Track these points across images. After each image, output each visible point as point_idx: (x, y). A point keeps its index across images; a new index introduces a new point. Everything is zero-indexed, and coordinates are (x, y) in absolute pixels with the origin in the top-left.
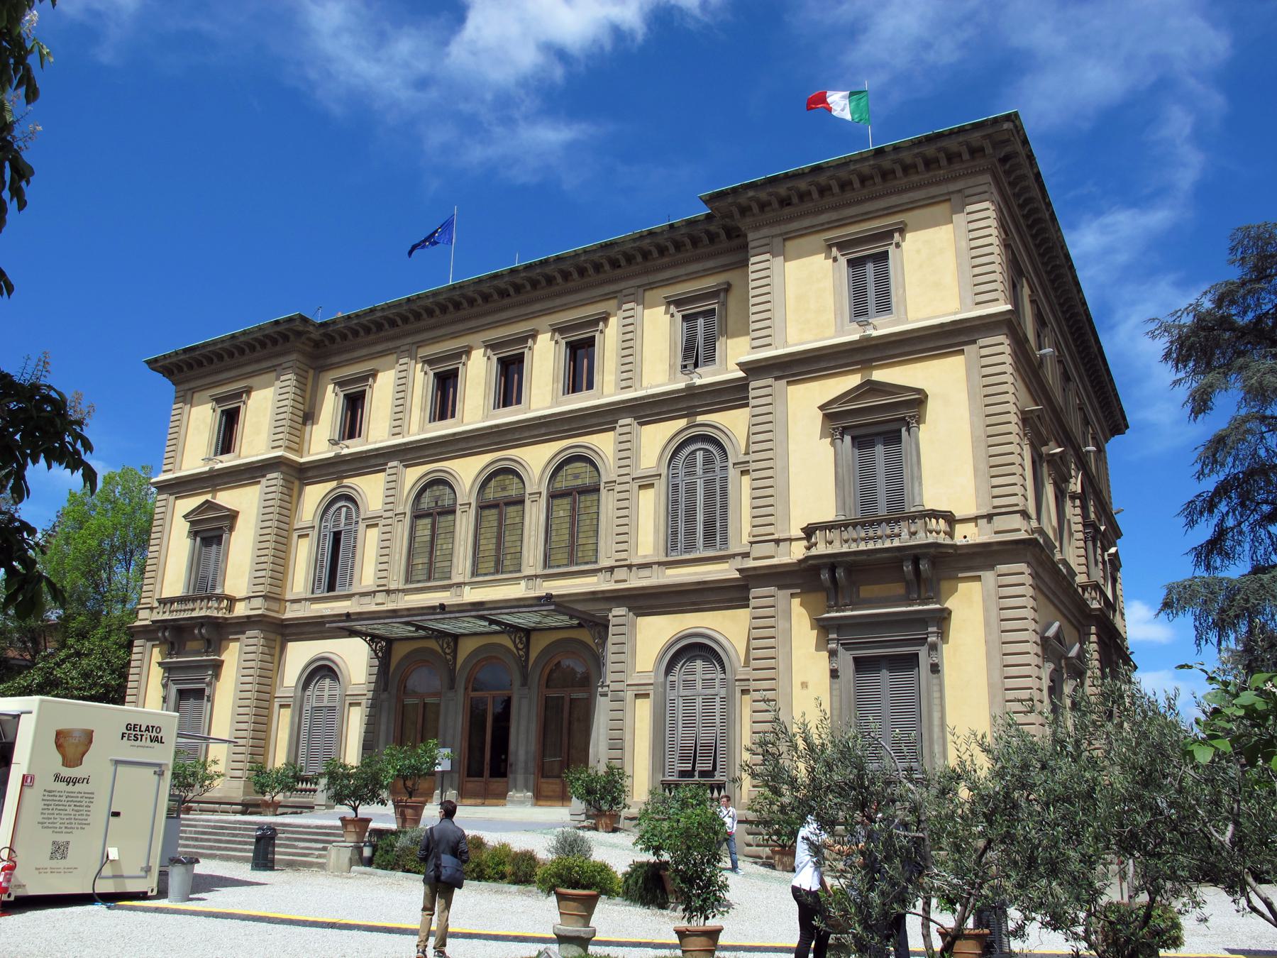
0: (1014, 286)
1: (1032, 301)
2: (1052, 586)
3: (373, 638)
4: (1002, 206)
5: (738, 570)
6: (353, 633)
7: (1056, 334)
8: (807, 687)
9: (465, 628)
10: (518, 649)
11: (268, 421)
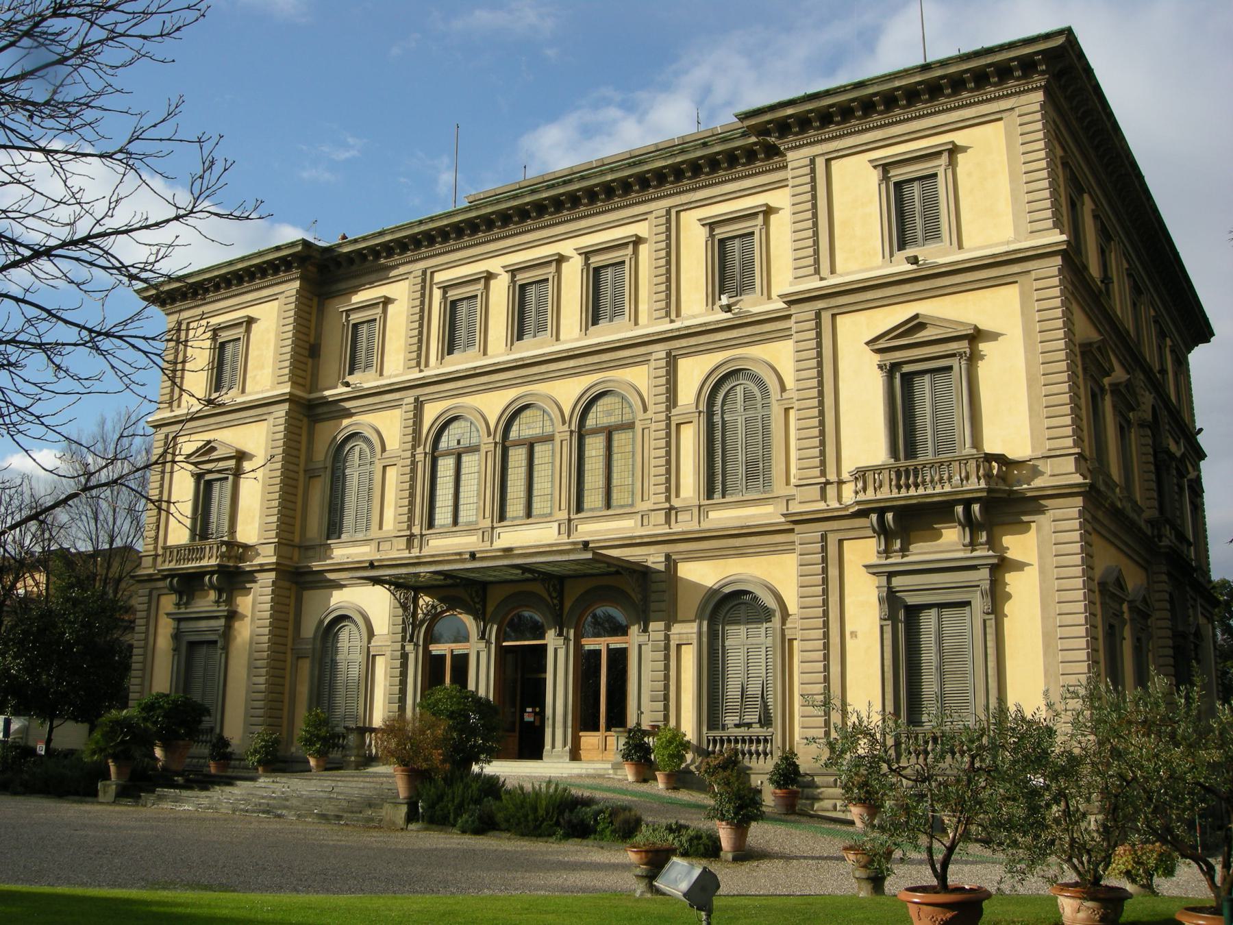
0: (1073, 205)
1: (1096, 217)
2: (1113, 527)
3: (396, 584)
4: (1058, 122)
5: (782, 515)
6: (376, 581)
7: (1125, 246)
8: (856, 636)
9: (495, 576)
10: (552, 598)
11: (271, 354)
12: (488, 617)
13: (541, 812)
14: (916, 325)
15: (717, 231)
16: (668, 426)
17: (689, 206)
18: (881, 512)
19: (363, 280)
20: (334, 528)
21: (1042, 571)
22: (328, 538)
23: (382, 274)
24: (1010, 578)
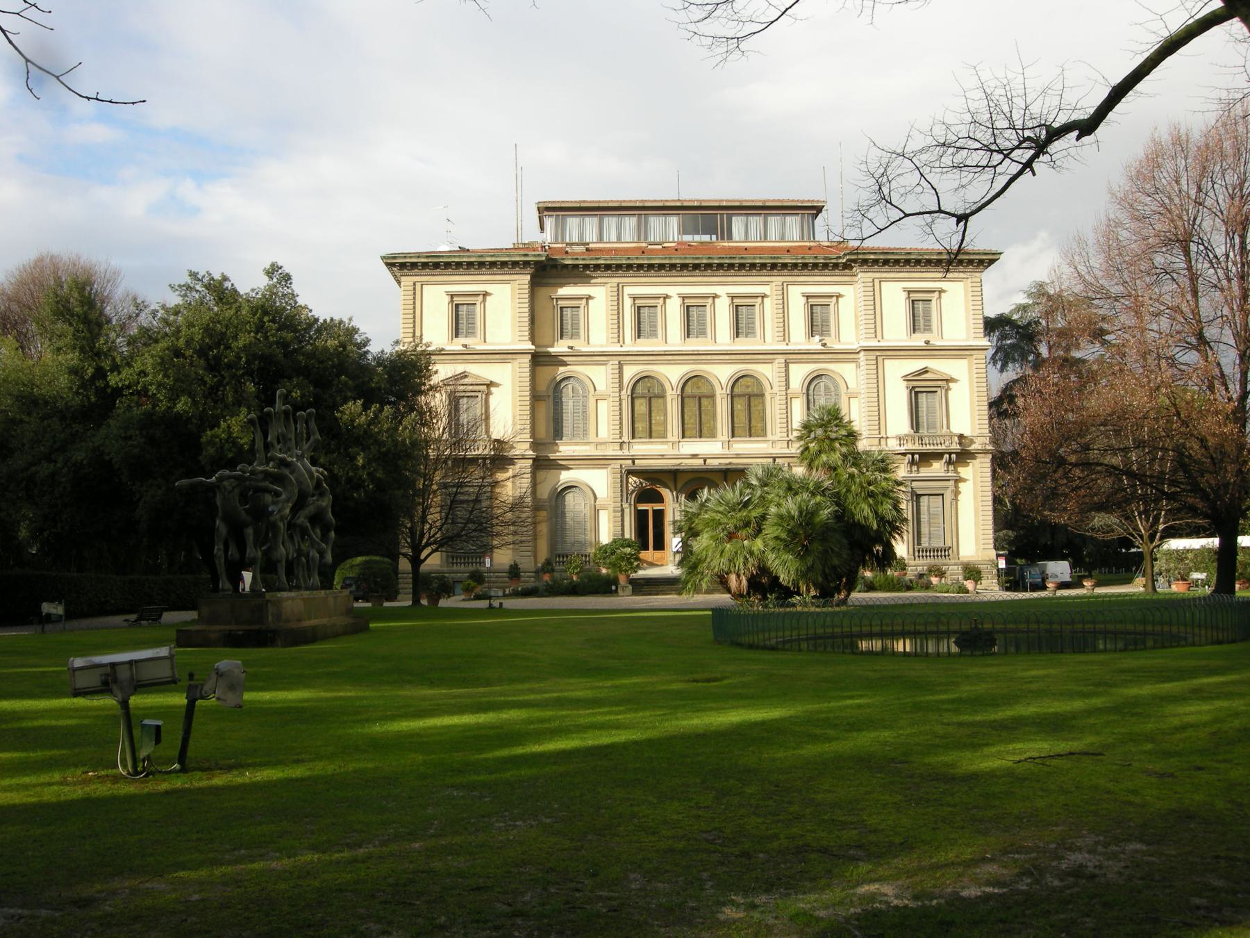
12: (678, 489)
13: (895, 581)
14: (464, 375)
15: (810, 300)
16: (787, 398)
17: (794, 283)
18: (913, 454)
19: (568, 280)
20: (558, 433)
21: (974, 483)
22: (555, 440)
23: (586, 280)
24: (961, 485)
